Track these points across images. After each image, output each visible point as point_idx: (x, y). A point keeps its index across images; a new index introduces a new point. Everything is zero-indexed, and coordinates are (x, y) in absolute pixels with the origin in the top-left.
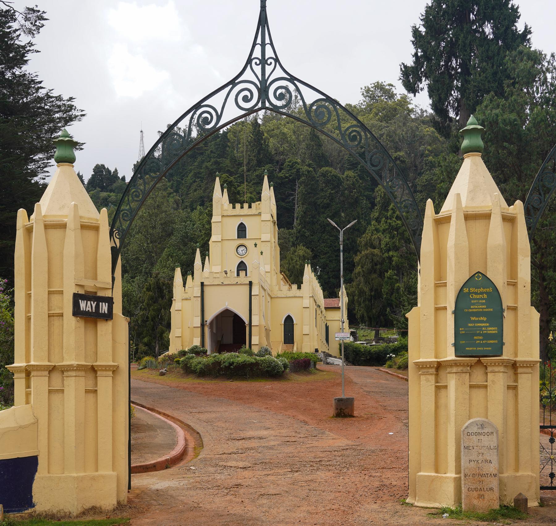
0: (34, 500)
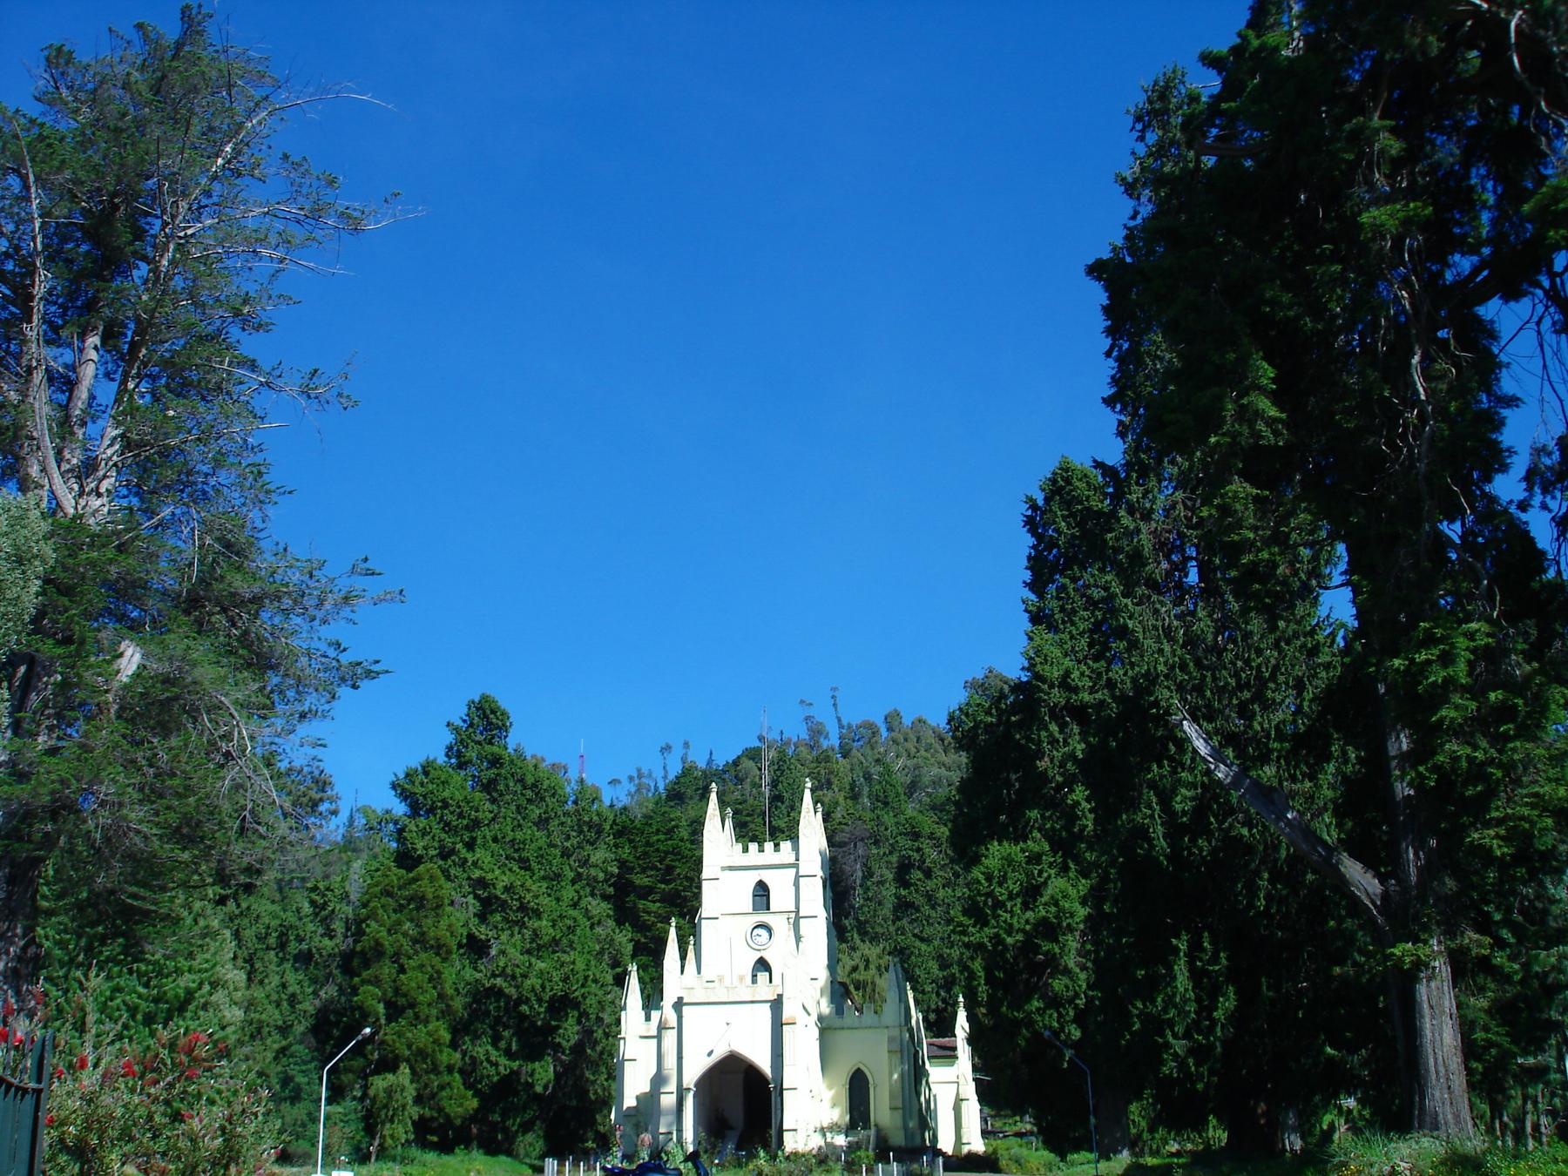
0: (1097, 294)
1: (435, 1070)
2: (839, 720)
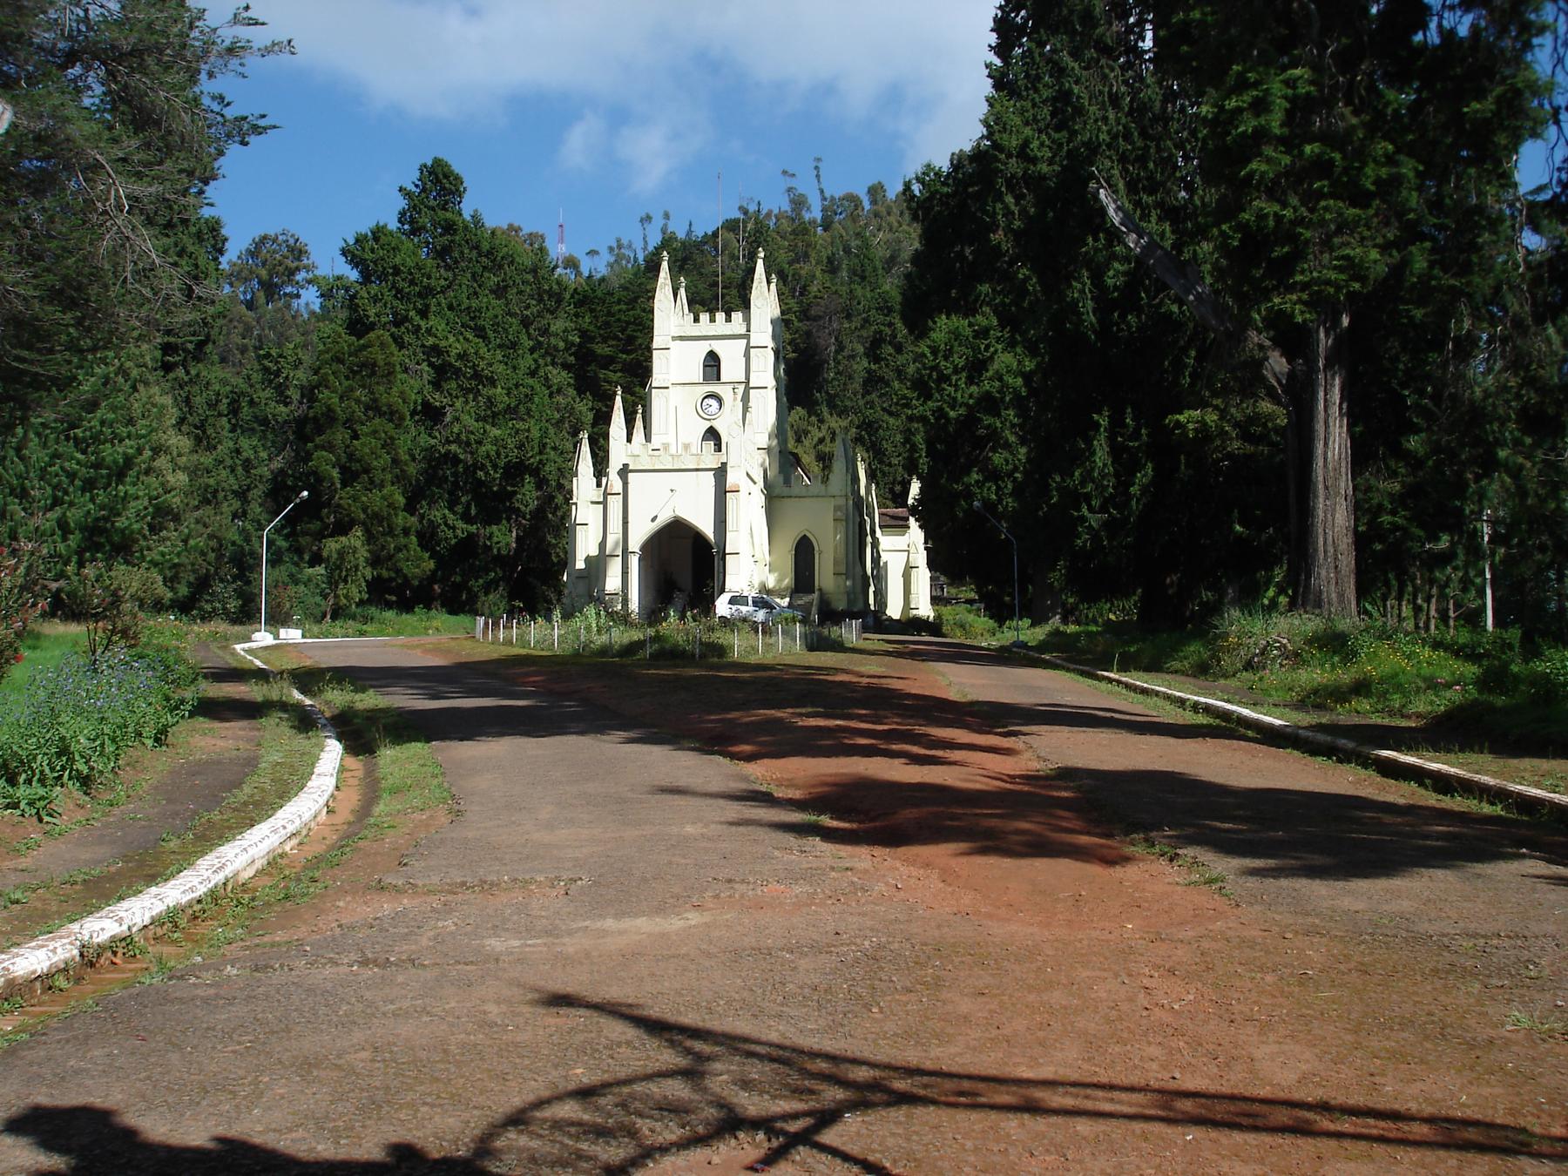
1: (390, 532)
2: (822, 191)
